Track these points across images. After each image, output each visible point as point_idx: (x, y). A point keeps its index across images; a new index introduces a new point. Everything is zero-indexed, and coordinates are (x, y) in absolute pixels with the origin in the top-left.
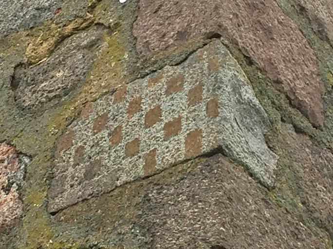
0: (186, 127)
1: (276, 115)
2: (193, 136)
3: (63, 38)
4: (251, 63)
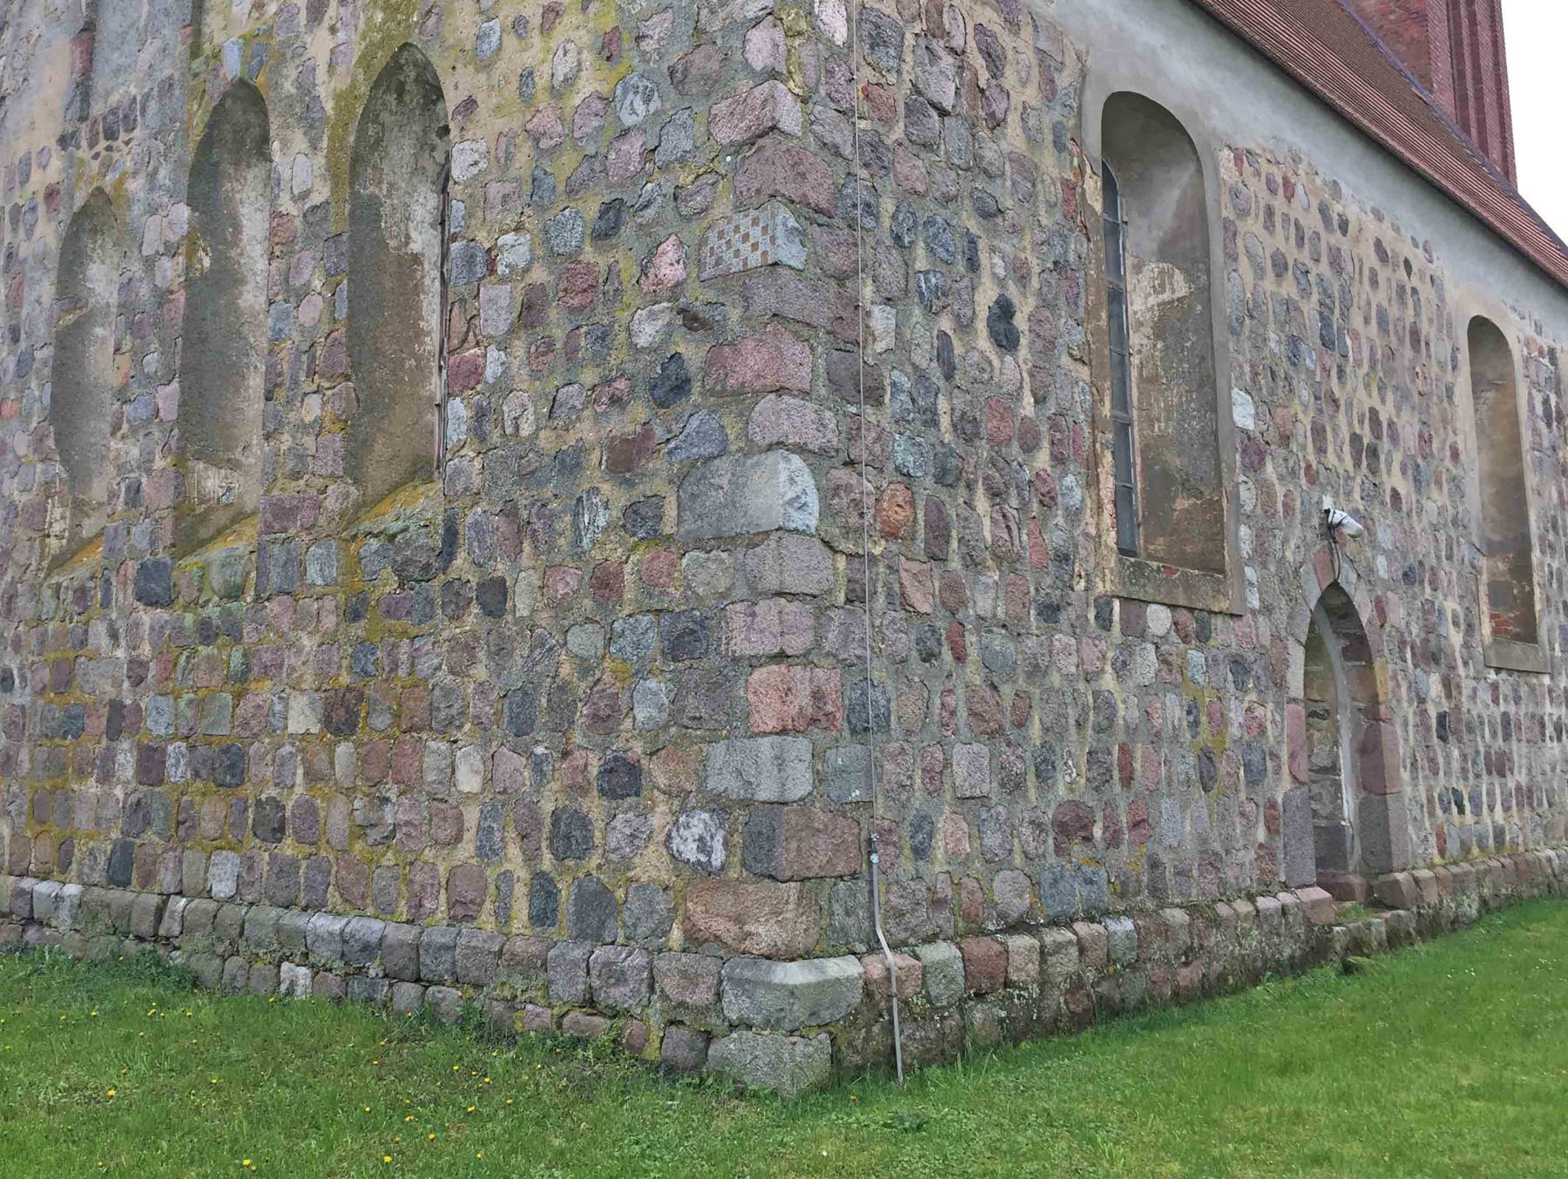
0: (762, 248)
1: (806, 223)
2: (765, 253)
3: (698, 176)
4: (792, 202)
